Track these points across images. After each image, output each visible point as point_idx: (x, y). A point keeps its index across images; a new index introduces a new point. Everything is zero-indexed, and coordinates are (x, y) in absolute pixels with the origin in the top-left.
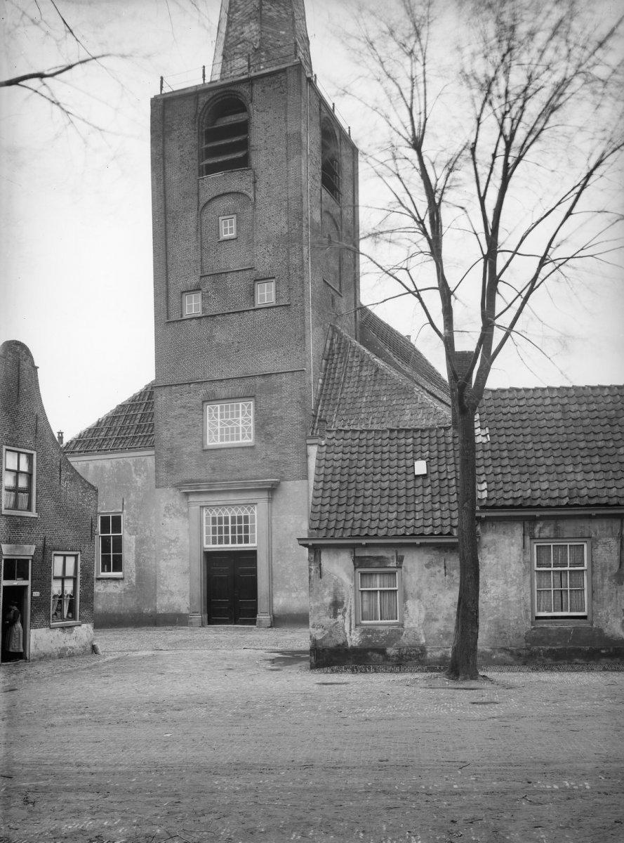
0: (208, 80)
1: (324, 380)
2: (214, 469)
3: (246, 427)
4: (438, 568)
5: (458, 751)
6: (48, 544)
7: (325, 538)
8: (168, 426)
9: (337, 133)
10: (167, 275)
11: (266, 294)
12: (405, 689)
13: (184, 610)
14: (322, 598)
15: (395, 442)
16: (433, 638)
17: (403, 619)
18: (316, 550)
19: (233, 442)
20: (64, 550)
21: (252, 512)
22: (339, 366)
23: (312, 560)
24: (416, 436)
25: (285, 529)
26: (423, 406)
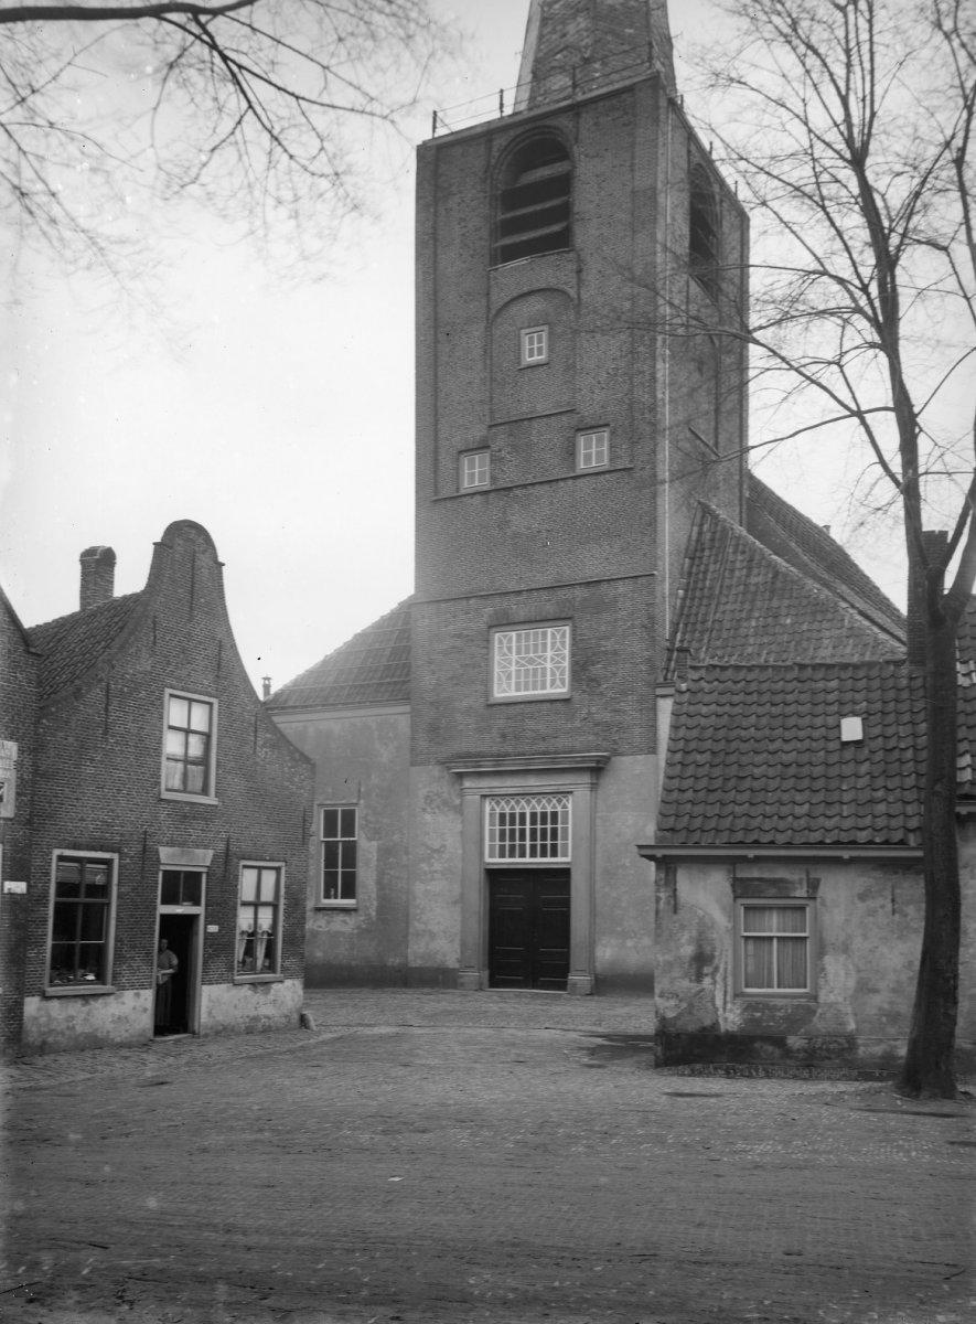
0: (508, 111)
1: (686, 591)
2: (504, 736)
3: (558, 668)
4: (880, 901)
5: (939, 1242)
6: (233, 849)
7: (683, 845)
8: (433, 667)
9: (716, 188)
10: (436, 425)
11: (593, 452)
12: (825, 1111)
13: (452, 962)
14: (678, 949)
15: (807, 686)
16: (870, 1022)
17: (816, 987)
18: (667, 865)
19: (536, 692)
20: (257, 857)
21: (565, 807)
22: (712, 568)
23: (663, 882)
24: (843, 676)
25: (618, 835)
26: (854, 633)
